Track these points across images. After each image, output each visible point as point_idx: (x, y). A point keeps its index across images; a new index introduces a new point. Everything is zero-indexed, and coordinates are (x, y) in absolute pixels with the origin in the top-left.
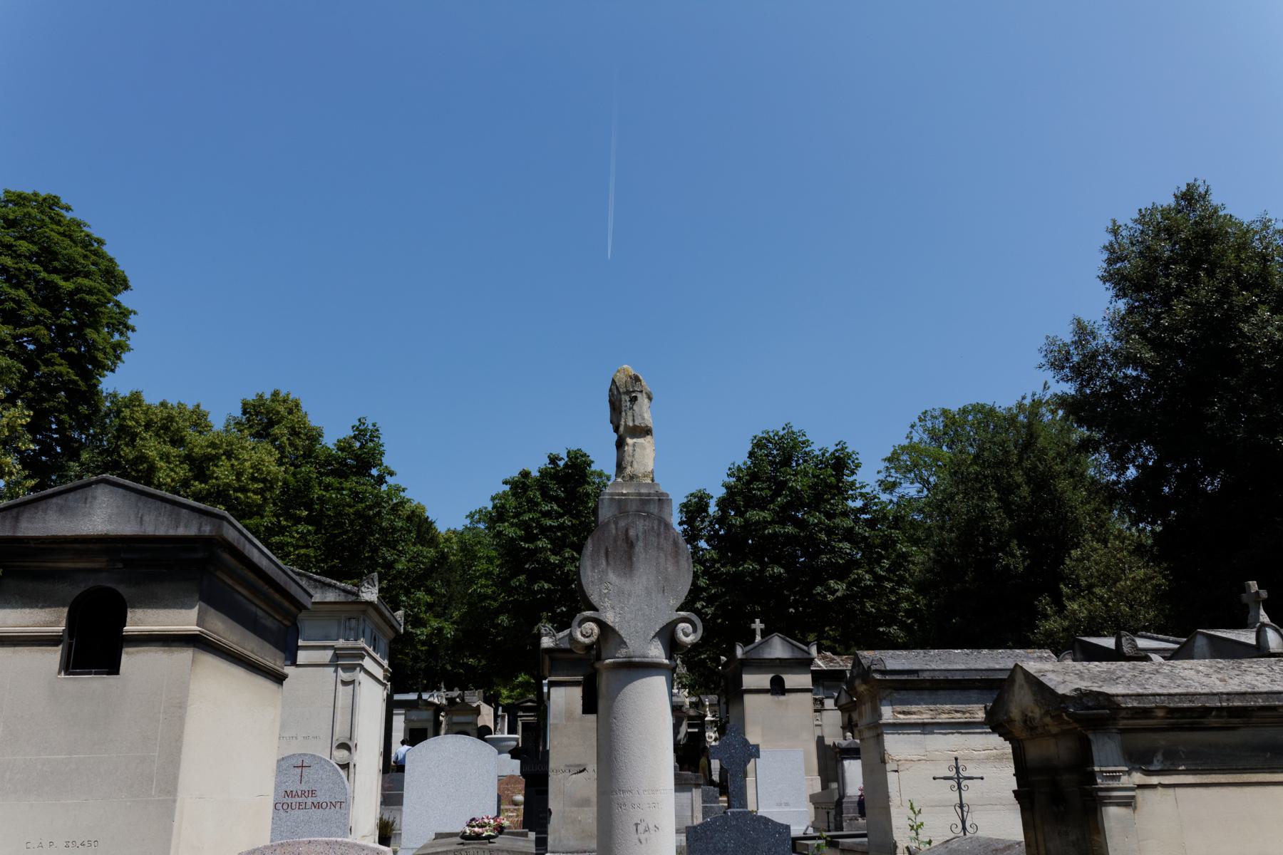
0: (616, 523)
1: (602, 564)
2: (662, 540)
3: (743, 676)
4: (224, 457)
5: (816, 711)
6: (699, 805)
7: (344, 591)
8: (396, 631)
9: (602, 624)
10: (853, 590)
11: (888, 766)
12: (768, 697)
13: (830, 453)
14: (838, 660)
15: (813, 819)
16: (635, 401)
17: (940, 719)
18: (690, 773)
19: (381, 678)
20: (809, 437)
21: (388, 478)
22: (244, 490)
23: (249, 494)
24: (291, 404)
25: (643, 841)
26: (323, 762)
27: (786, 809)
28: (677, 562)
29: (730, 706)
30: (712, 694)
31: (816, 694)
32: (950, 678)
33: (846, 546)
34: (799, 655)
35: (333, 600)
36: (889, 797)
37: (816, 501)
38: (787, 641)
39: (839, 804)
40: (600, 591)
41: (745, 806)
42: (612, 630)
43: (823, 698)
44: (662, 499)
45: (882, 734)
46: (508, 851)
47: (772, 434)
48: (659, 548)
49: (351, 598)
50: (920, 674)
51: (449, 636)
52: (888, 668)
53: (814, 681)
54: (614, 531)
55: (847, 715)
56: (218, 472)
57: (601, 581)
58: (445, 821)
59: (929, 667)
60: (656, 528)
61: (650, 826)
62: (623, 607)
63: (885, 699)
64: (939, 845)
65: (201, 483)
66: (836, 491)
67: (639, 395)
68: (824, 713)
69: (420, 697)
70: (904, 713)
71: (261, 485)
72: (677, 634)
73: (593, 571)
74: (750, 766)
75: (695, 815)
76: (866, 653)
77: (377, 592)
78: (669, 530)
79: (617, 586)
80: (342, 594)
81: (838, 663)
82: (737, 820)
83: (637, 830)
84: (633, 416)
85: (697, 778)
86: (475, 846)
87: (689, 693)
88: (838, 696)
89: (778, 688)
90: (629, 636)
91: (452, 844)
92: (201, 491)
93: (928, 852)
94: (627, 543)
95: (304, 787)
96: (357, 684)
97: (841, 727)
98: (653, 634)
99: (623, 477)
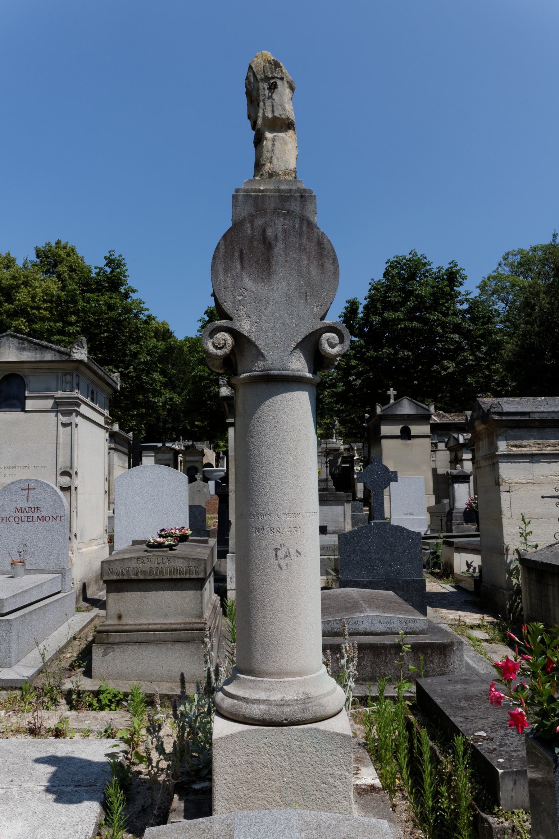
0: (252, 222)
1: (236, 267)
2: (305, 242)
3: (337, 543)
4: (22, 286)
5: (432, 451)
7: (59, 352)
8: (114, 389)
9: (236, 334)
10: (460, 367)
11: (501, 487)
12: (399, 441)
13: (445, 269)
14: (448, 416)
15: (429, 523)
16: (274, 89)
17: (546, 450)
18: (343, 493)
19: (103, 423)
20: (429, 259)
21: (131, 294)
22: (38, 308)
23: (41, 311)
24: (68, 250)
25: (284, 567)
26: (44, 486)
27: (411, 517)
28: (322, 265)
29: (372, 449)
30: (359, 442)
31: (432, 440)
32: (556, 418)
33: (456, 337)
34: (421, 412)
35: (50, 359)
36: (501, 511)
37: (435, 306)
38: (414, 402)
39: (450, 514)
40: (234, 297)
42: (248, 340)
43: (437, 443)
44: (305, 195)
45: (498, 463)
46: (183, 558)
47: (401, 258)
48: (302, 249)
49: (65, 358)
50: (531, 415)
51: (178, 403)
52: (504, 411)
53: (432, 430)
54: (249, 231)
55: (454, 454)
56: (19, 296)
57: (235, 286)
58: (148, 530)
59: (538, 410)
60: (297, 226)
61: (291, 551)
62: (260, 316)
63: (501, 435)
64: (544, 548)
65: (9, 304)
66: (449, 297)
67: (279, 83)
68: (438, 452)
69: (164, 445)
70: (516, 446)
71: (49, 305)
72: (321, 345)
73: (226, 275)
75: (346, 521)
76: (485, 400)
77: (86, 352)
78: (312, 229)
79: (253, 292)
80: (57, 354)
81: (448, 418)
82: (379, 528)
83: (276, 555)
84: (273, 106)
85: (348, 496)
86: (156, 554)
87: (344, 442)
88: (448, 441)
89: (406, 435)
90: (267, 347)
91: (138, 551)
92: (9, 309)
93: (535, 554)
94: (264, 244)
95: (30, 505)
96: (74, 426)
97: (450, 462)
98: (294, 344)
99: (262, 175)
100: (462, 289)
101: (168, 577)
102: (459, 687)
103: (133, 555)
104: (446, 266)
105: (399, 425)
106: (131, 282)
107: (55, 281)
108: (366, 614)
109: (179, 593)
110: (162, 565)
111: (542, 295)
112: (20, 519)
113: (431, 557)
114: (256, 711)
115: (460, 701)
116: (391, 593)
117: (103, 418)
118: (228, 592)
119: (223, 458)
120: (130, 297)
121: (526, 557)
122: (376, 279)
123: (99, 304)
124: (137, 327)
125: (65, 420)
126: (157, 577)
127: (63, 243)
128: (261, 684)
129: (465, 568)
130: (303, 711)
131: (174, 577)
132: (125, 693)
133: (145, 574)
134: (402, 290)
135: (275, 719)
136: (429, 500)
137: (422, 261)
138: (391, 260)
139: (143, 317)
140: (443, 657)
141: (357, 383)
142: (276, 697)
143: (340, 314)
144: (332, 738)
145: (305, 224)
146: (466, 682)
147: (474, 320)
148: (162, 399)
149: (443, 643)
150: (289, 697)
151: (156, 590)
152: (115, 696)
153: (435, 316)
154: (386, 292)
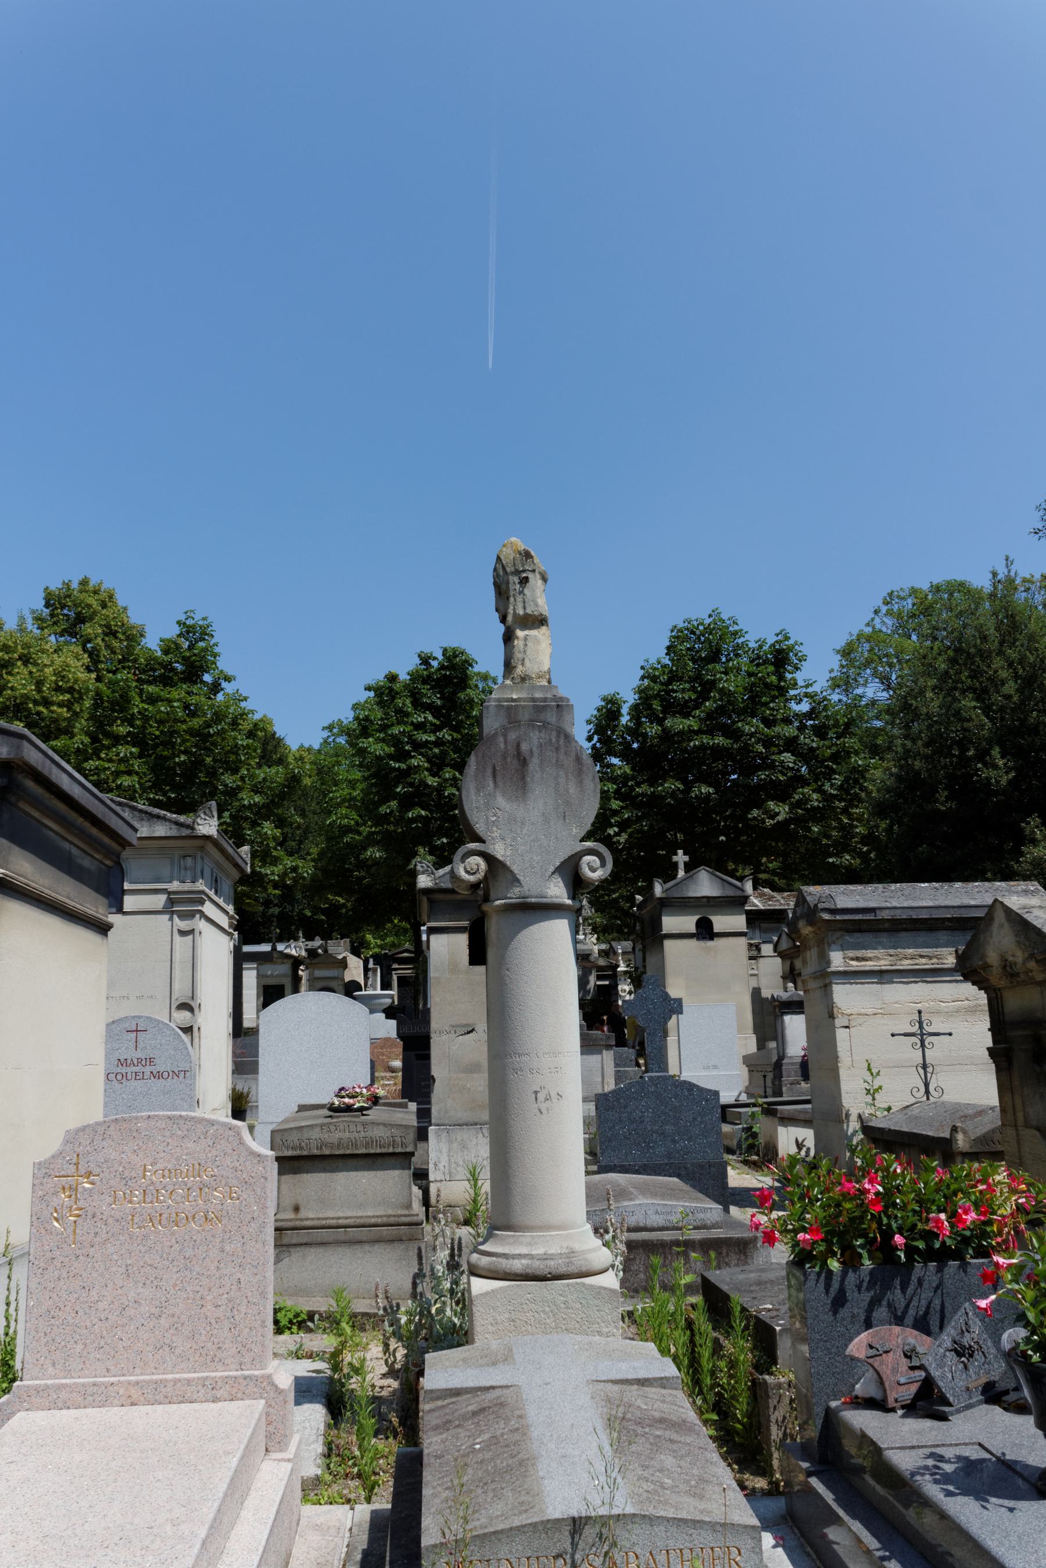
0: (505, 736)
2: (562, 757)
5: (751, 958)
6: (610, 1069)
7: (177, 823)
8: (242, 870)
12: (693, 943)
14: (779, 898)
15: (747, 1084)
20: (742, 625)
22: (47, 703)
24: (103, 596)
26: (161, 1025)
27: (715, 1073)
29: (648, 955)
30: (625, 940)
31: (751, 939)
33: (788, 757)
34: (730, 892)
35: (163, 834)
37: (753, 707)
39: (778, 1065)
40: (487, 818)
41: (666, 1069)
42: (502, 865)
45: (831, 983)
46: (384, 1125)
47: (695, 623)
48: (559, 765)
49: (185, 832)
50: (878, 912)
51: (305, 875)
54: (502, 746)
55: (788, 963)
56: (12, 681)
59: (889, 905)
60: (554, 740)
63: (834, 943)
67: (531, 576)
68: (761, 960)
70: (857, 959)
74: (672, 1023)
78: (570, 743)
80: (174, 827)
87: (598, 939)
89: (705, 931)
98: (552, 869)
100: (800, 677)
101: (363, 1151)
102: (752, 1275)
103: (314, 1122)
104: (771, 639)
105: (694, 915)
106: (224, 664)
107: (77, 653)
108: (638, 1202)
109: (380, 1173)
110: (356, 1135)
111: (929, 695)
112: (125, 1076)
113: (744, 1136)
114: (518, 1266)
115: (750, 1285)
116: (676, 1180)
117: (226, 918)
118: (431, 1185)
119: (375, 970)
120: (222, 689)
121: (870, 1124)
122: (653, 660)
123: (172, 707)
124: (236, 745)
125: (184, 925)
126: (348, 1152)
127: (92, 584)
128: (521, 1239)
129: (793, 1150)
130: (568, 1264)
131: (372, 1151)
132: (309, 1311)
133: (332, 1148)
134: (697, 677)
135: (538, 1273)
136: (746, 1044)
137: (731, 629)
138: (679, 627)
139: (246, 726)
140: (743, 1258)
141: (622, 840)
142: (538, 1250)
143: (588, 717)
144: (599, 1293)
145: (562, 738)
146: (763, 1270)
147: (820, 732)
148: (278, 869)
149: (742, 1238)
150: (551, 1251)
151: (348, 1170)
152: (297, 1315)
153: (751, 726)
154: (670, 682)
